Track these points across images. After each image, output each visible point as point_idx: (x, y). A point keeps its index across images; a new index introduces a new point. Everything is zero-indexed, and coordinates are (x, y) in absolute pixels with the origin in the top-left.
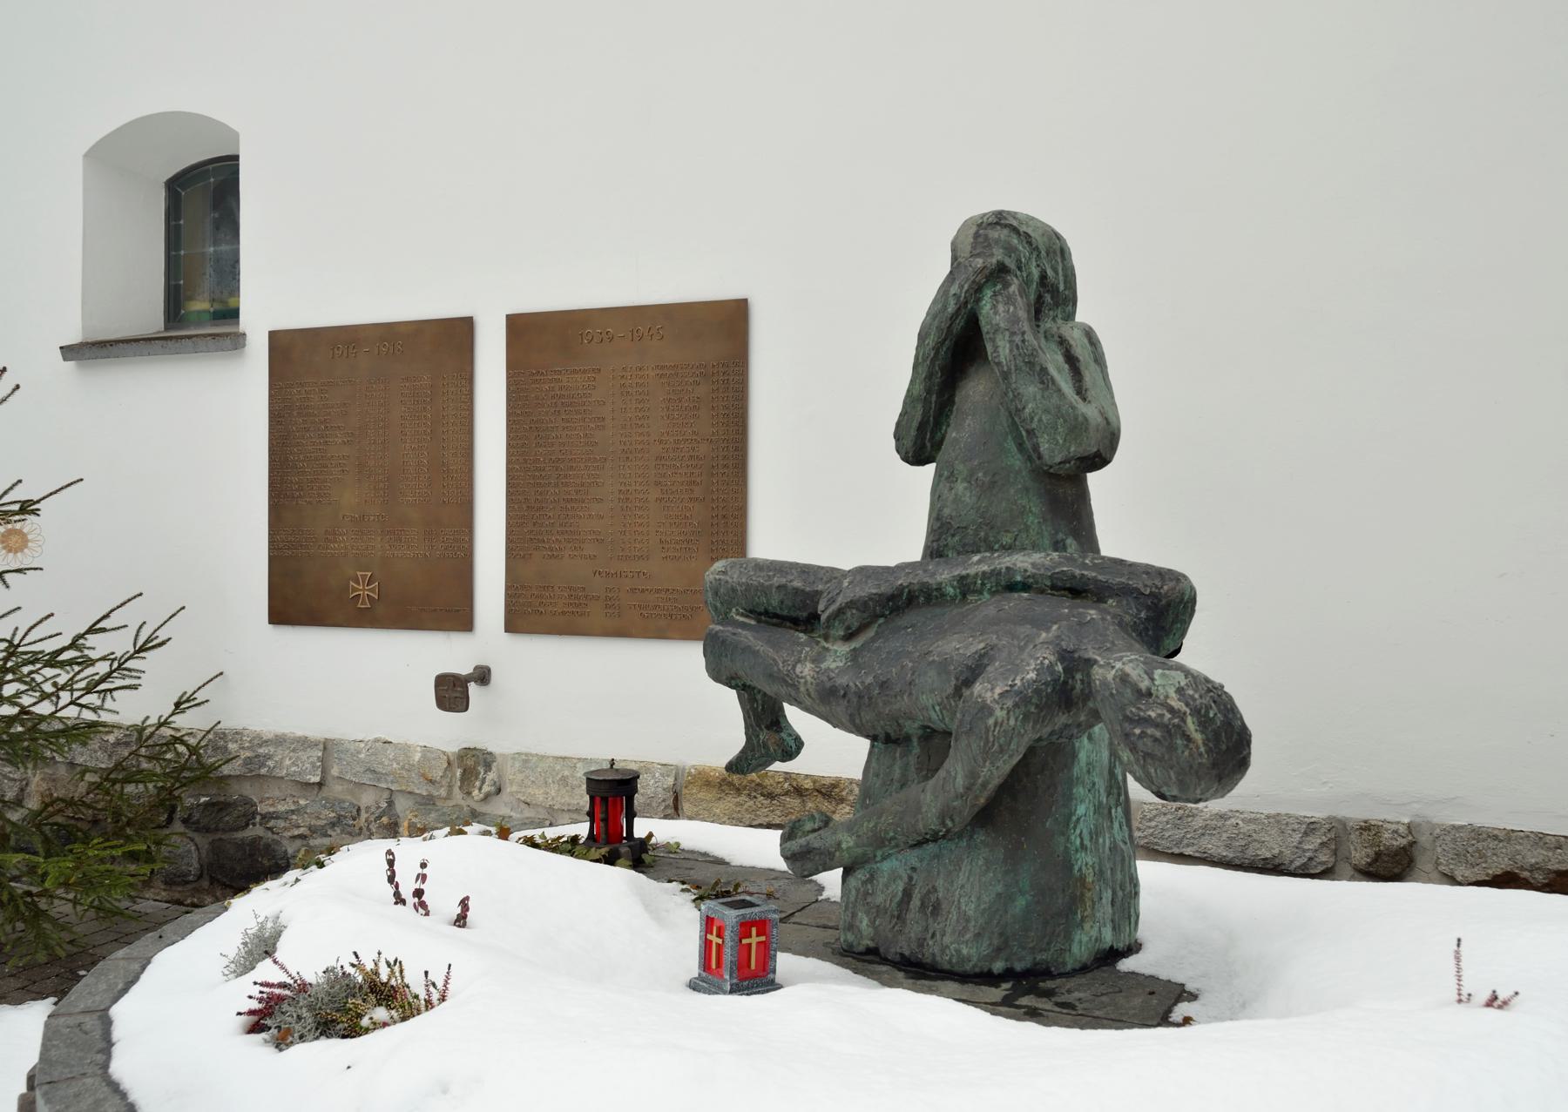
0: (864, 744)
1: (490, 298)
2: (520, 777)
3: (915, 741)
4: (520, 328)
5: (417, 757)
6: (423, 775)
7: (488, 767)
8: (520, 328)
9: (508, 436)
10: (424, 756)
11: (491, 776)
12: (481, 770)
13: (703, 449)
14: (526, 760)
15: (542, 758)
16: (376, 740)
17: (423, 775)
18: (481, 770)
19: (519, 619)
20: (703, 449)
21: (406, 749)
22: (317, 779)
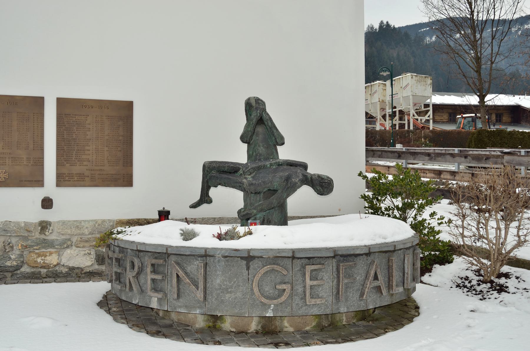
0: (240, 195)
1: (51, 87)
2: (62, 227)
3: (43, 236)
4: (61, 103)
5: (23, 225)
6: (26, 230)
7: (50, 226)
8: (61, 103)
9: (57, 128)
10: (25, 225)
11: (51, 228)
12: (48, 226)
13: (121, 138)
14: (64, 223)
15: (69, 221)
16: (6, 221)
17: (26, 230)
18: (48, 226)
19: (62, 180)
20: (121, 138)
21: (18, 223)
22: (308, 303)
